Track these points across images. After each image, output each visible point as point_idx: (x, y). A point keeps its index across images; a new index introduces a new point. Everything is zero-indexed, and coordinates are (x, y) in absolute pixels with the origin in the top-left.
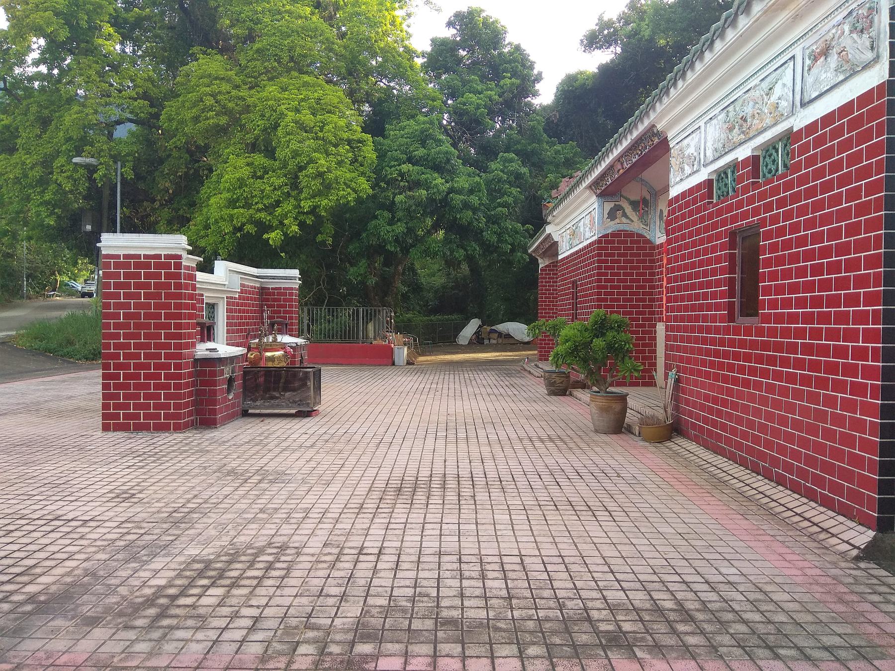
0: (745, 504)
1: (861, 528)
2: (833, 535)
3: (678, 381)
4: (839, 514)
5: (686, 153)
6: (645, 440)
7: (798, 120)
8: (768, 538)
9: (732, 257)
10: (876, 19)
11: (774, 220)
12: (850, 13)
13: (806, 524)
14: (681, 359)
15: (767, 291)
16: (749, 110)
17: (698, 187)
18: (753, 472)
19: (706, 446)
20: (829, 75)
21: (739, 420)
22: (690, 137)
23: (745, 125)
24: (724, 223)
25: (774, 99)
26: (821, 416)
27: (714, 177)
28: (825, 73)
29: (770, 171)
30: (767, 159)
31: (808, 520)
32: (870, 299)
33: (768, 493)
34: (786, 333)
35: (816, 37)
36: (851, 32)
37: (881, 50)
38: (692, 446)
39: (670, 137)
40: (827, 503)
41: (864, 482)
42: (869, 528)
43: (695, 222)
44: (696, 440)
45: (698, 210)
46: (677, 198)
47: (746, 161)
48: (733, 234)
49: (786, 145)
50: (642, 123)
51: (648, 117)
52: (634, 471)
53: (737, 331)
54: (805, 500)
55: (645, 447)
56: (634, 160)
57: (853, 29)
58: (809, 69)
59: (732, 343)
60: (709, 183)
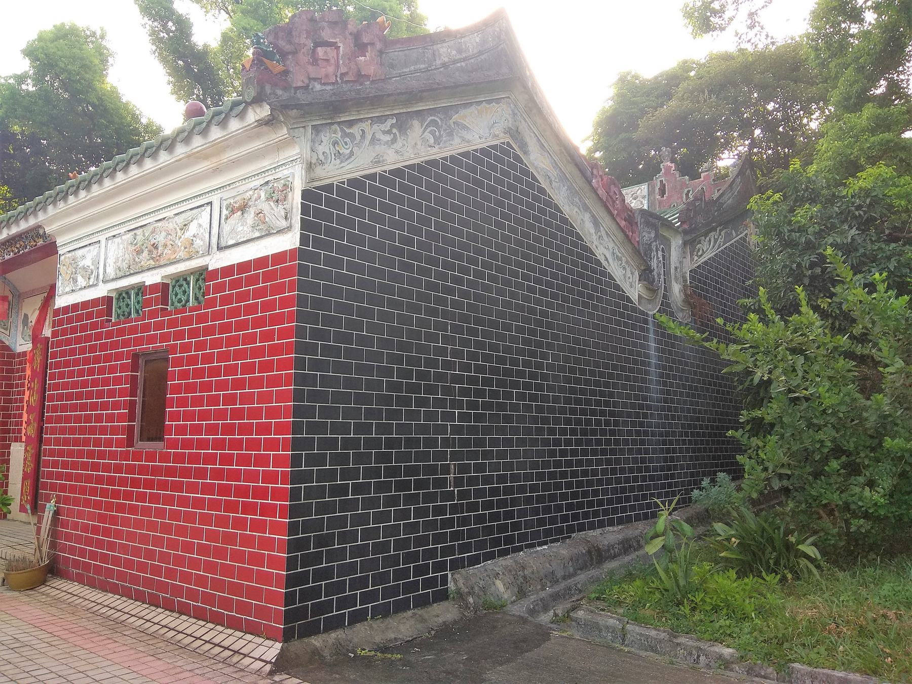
0: (151, 642)
1: (269, 643)
2: (245, 656)
3: (57, 513)
4: (246, 633)
5: (81, 264)
6: (12, 589)
7: (213, 261)
8: (188, 674)
9: (134, 379)
10: (290, 195)
11: (186, 348)
12: (267, 183)
13: (217, 650)
14: (63, 488)
15: (175, 416)
16: (160, 238)
17: (95, 302)
18: (152, 605)
19: (92, 584)
20: (245, 228)
21: (136, 552)
22: (86, 249)
23: (155, 252)
24: (126, 343)
25: (189, 234)
26: (230, 539)
27: (114, 295)
28: (242, 226)
29: (180, 301)
30: (177, 288)
31: (218, 645)
32: (280, 428)
33: (172, 625)
34: (194, 459)
35: (233, 193)
36: (267, 199)
37: (293, 222)
38: (75, 588)
39: (59, 242)
40: (235, 624)
41: (271, 597)
42: (276, 641)
43: (88, 338)
44: (80, 580)
45: (94, 326)
46: (66, 309)
47: (154, 288)
48: (135, 357)
49: (198, 280)
50: (26, 220)
51: (36, 216)
52: (11, 631)
53: (137, 456)
54: (211, 625)
55: (15, 599)
56: (7, 257)
57: (269, 198)
58: (227, 219)
59: (131, 469)
60: (108, 300)
